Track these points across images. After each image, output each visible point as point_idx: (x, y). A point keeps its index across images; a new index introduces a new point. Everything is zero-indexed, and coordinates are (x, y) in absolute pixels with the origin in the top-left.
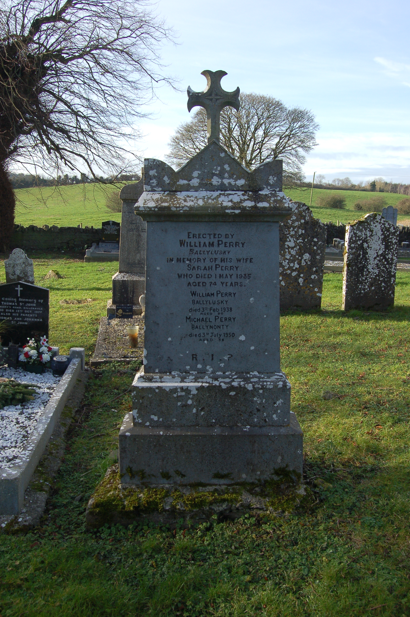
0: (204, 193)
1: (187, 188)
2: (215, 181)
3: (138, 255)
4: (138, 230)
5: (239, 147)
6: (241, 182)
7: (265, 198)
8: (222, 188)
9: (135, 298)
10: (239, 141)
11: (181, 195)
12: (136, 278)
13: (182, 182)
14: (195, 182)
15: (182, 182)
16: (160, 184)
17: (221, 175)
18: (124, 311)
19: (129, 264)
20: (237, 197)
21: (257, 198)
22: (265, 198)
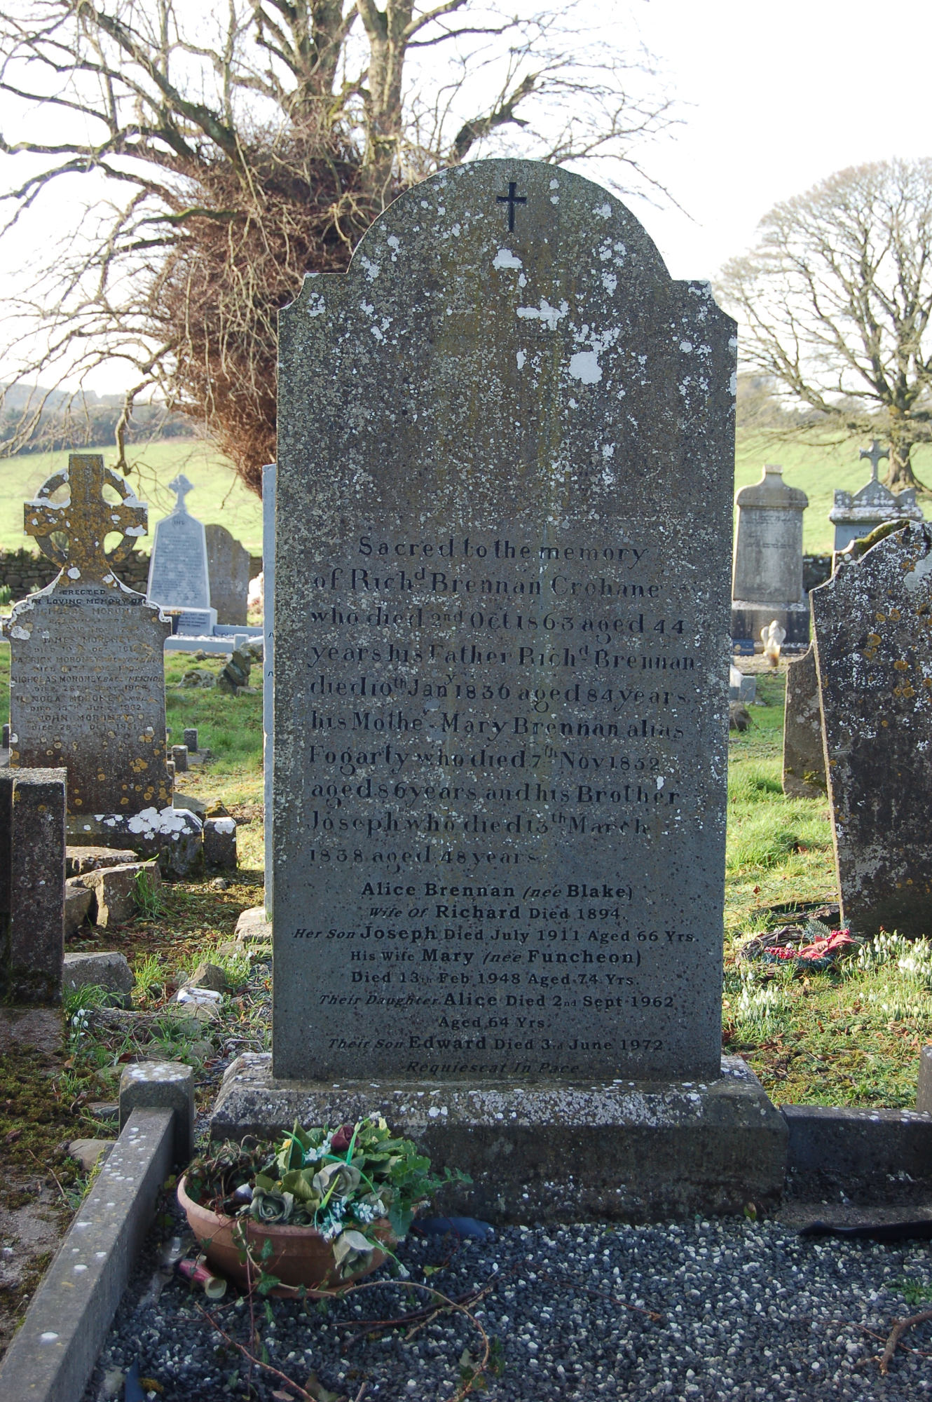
0: (869, 509)
1: (859, 506)
2: (876, 502)
3: (758, 578)
4: (758, 545)
5: (896, 320)
6: (891, 502)
7: (905, 511)
8: (880, 505)
9: (754, 633)
10: (894, 302)
11: (855, 510)
12: (755, 607)
13: (856, 502)
14: (864, 502)
15: (856, 502)
16: (844, 503)
17: (879, 498)
18: (743, 646)
19: (745, 589)
20: (889, 511)
21: (900, 511)
22: (905, 511)
